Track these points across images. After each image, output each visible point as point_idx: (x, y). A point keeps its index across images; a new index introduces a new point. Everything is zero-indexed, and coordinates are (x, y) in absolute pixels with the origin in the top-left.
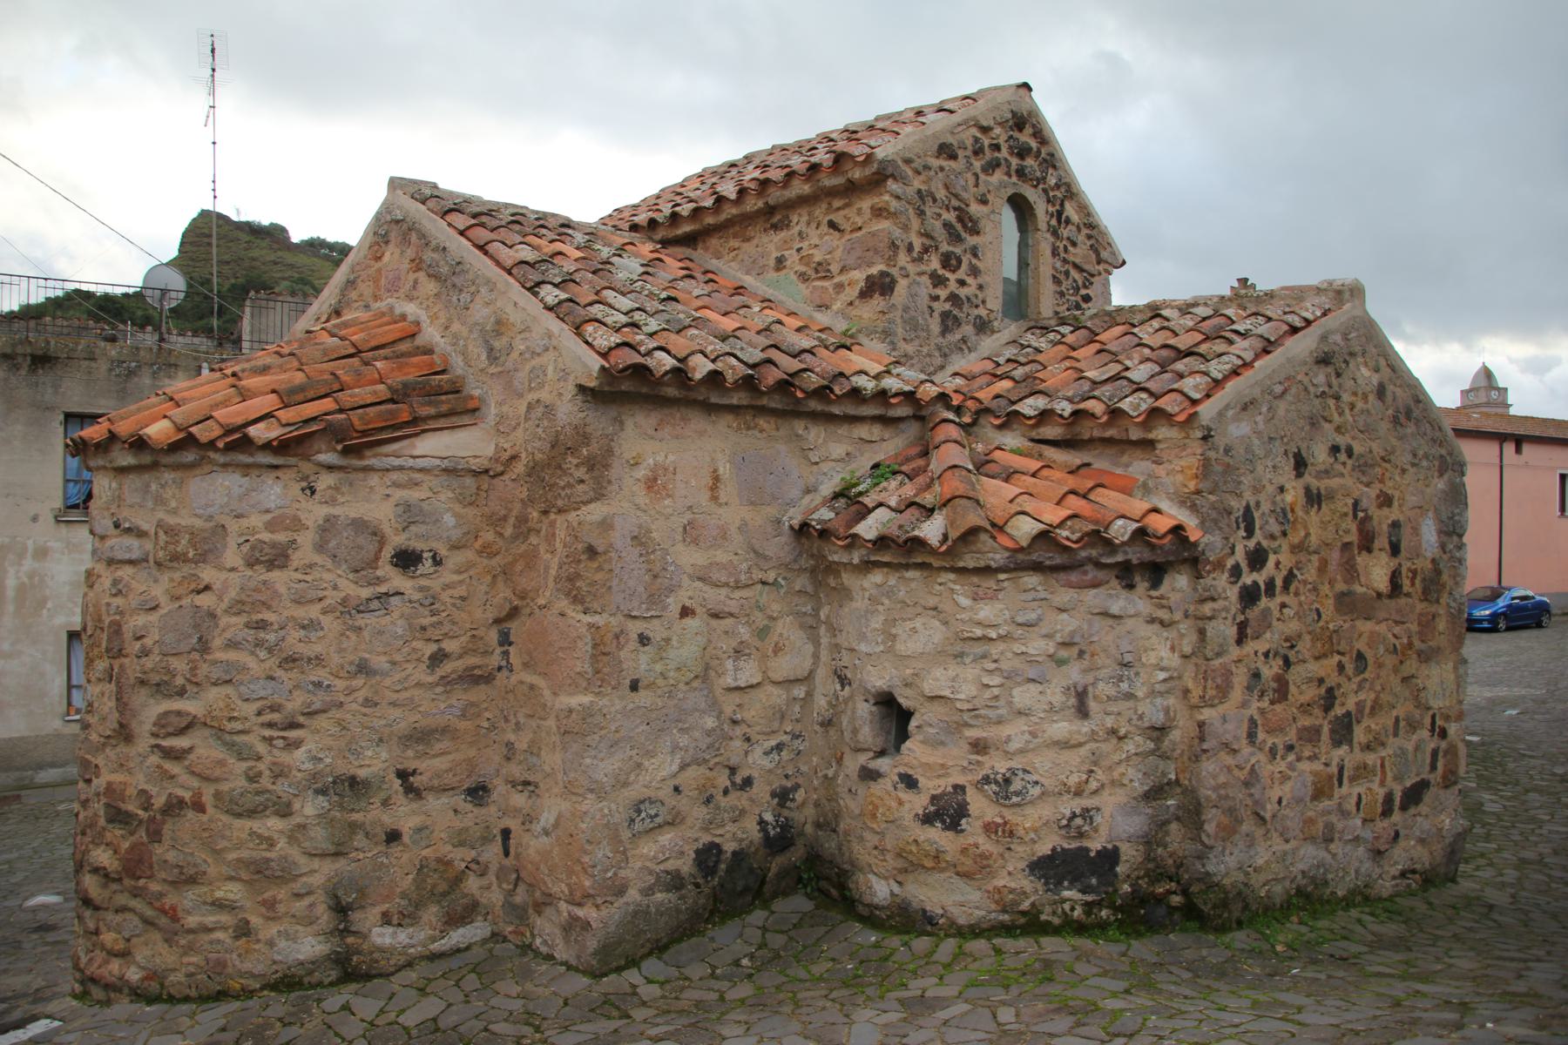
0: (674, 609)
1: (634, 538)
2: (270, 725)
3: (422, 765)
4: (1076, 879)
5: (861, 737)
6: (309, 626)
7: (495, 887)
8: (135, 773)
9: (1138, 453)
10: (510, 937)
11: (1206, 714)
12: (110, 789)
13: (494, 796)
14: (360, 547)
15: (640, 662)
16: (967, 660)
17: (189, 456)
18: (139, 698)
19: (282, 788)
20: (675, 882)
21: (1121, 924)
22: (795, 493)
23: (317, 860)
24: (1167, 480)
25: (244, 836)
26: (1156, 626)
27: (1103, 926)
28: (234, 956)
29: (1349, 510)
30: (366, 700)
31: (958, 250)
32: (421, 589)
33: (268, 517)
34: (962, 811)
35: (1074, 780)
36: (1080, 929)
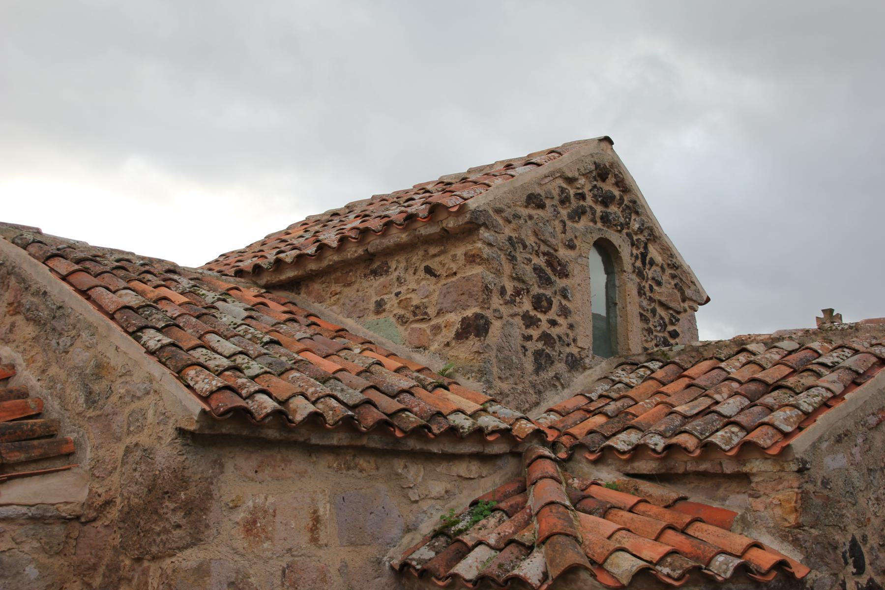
22: (395, 532)
31: (548, 293)
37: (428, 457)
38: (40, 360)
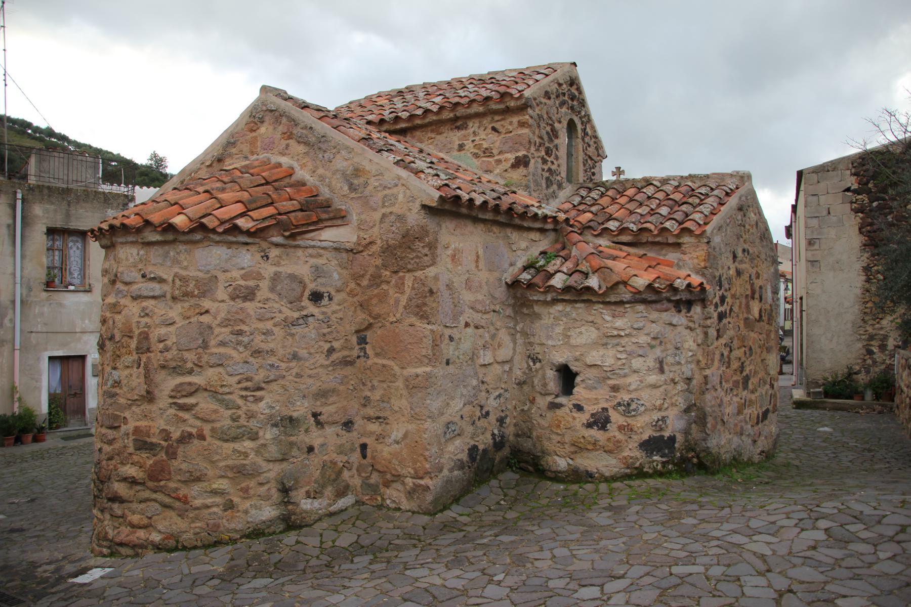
0: (463, 323)
1: (447, 285)
2: (246, 389)
3: (324, 410)
4: (659, 450)
5: (549, 388)
6: (267, 333)
7: (356, 476)
8: (160, 420)
9: (671, 249)
10: (367, 502)
11: (707, 372)
12: (137, 430)
13: (356, 426)
14: (294, 290)
15: (449, 350)
16: (609, 347)
17: (198, 236)
18: (160, 376)
19: (253, 424)
20: (461, 465)
21: (677, 471)
22: (506, 266)
23: (271, 464)
24: (689, 262)
25: (230, 452)
26: (688, 330)
27: (670, 473)
28: (224, 521)
29: (748, 279)
30: (297, 374)
31: (551, 146)
32: (323, 313)
33: (243, 272)
34: (607, 420)
35: (658, 403)
36: (661, 474)
37: (520, 228)
38: (310, 166)
